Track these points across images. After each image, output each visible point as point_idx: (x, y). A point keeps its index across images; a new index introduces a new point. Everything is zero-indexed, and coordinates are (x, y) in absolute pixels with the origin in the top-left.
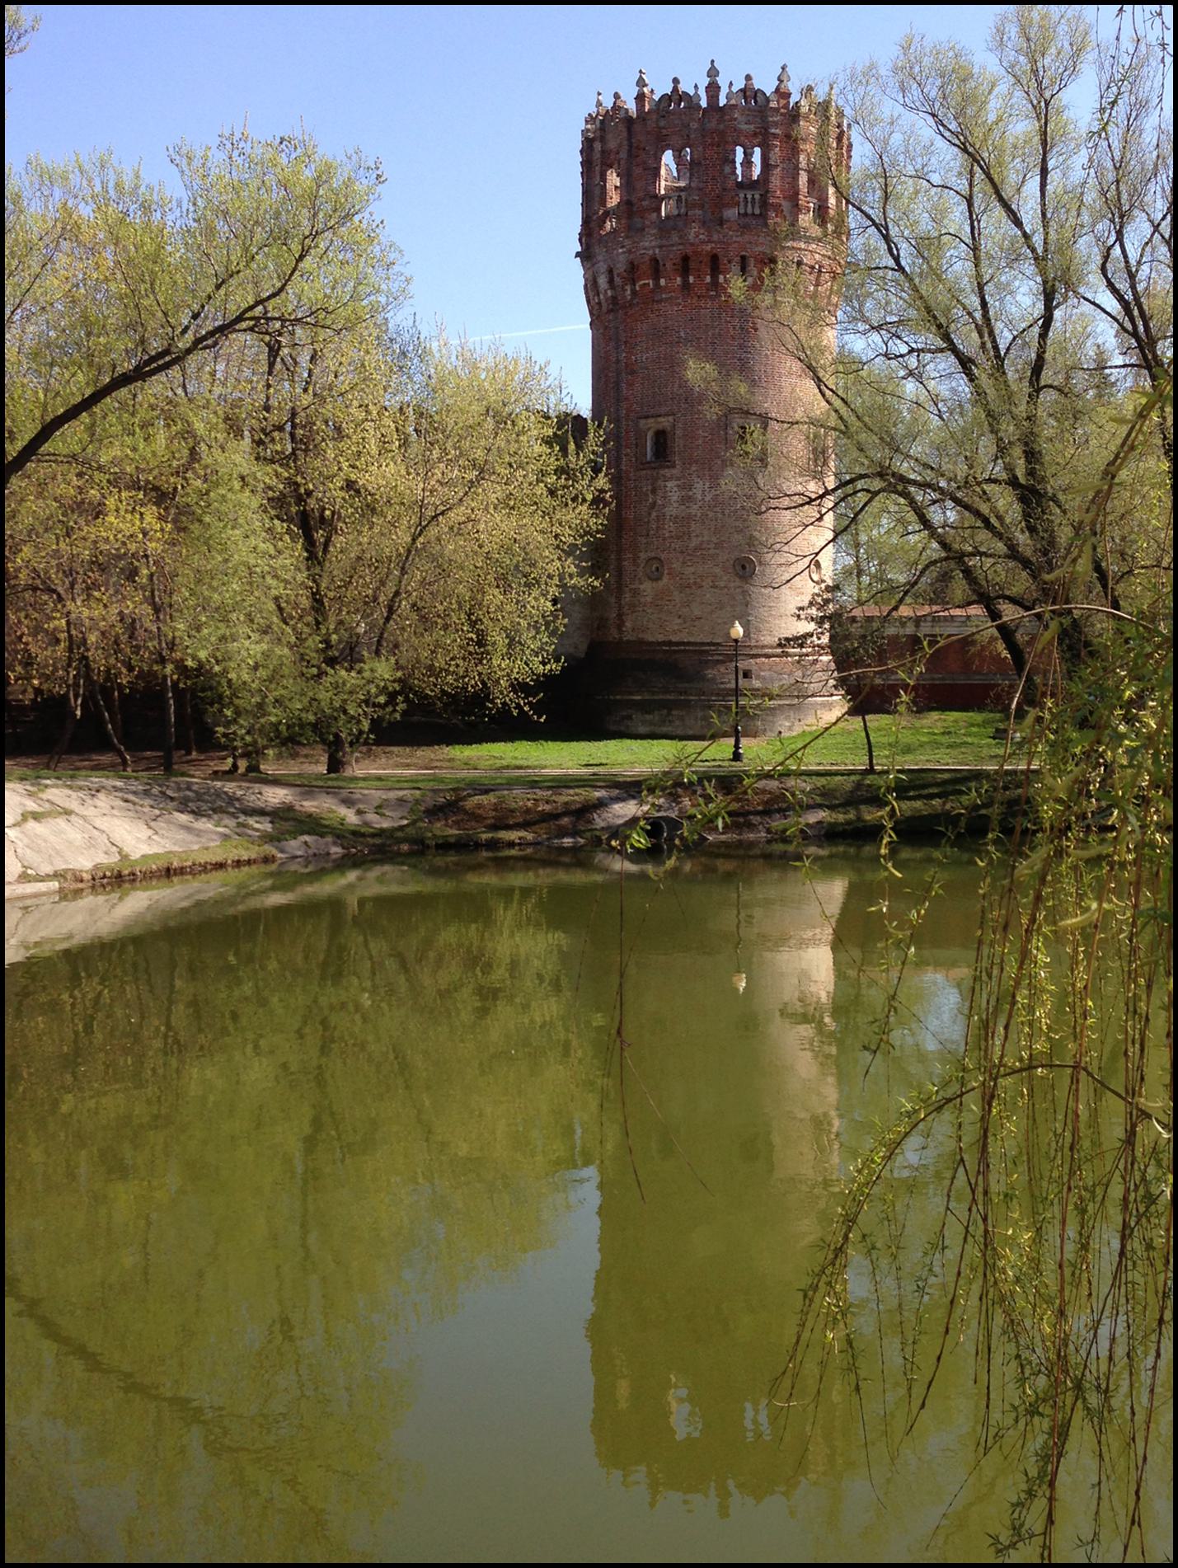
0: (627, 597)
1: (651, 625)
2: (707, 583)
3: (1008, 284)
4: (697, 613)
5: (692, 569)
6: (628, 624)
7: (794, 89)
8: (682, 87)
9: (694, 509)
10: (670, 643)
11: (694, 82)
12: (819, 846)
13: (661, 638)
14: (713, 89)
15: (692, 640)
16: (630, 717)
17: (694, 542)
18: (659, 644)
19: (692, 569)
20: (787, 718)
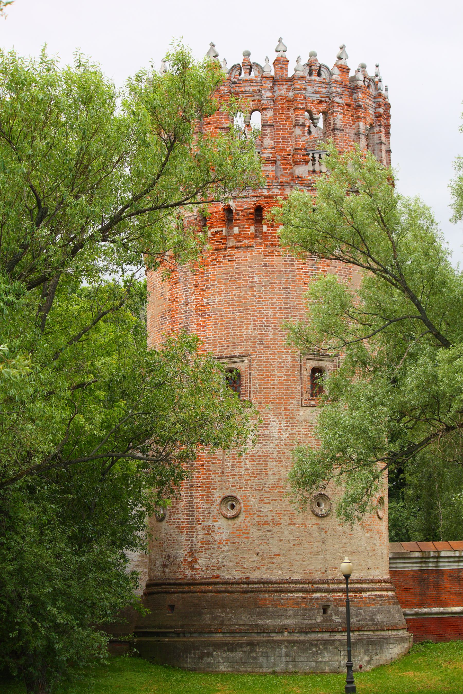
0: (200, 535)
1: (227, 563)
2: (284, 521)
3: (45, 586)
4: (275, 550)
5: (270, 507)
6: (202, 562)
7: (353, 65)
8: (252, 60)
9: (271, 447)
10: (248, 582)
11: (264, 57)
12: (419, 608)
13: (238, 575)
14: (281, 62)
15: (270, 577)
16: (209, 655)
17: (271, 481)
18: (237, 583)
19: (270, 507)
20: (366, 652)
